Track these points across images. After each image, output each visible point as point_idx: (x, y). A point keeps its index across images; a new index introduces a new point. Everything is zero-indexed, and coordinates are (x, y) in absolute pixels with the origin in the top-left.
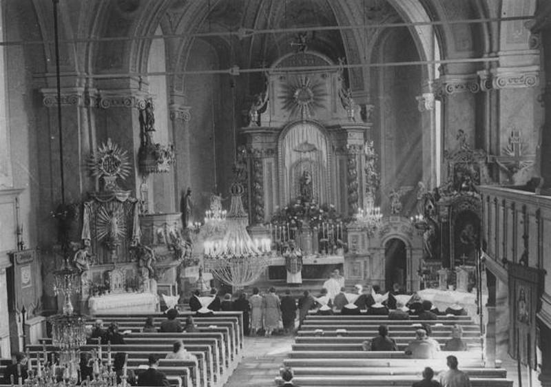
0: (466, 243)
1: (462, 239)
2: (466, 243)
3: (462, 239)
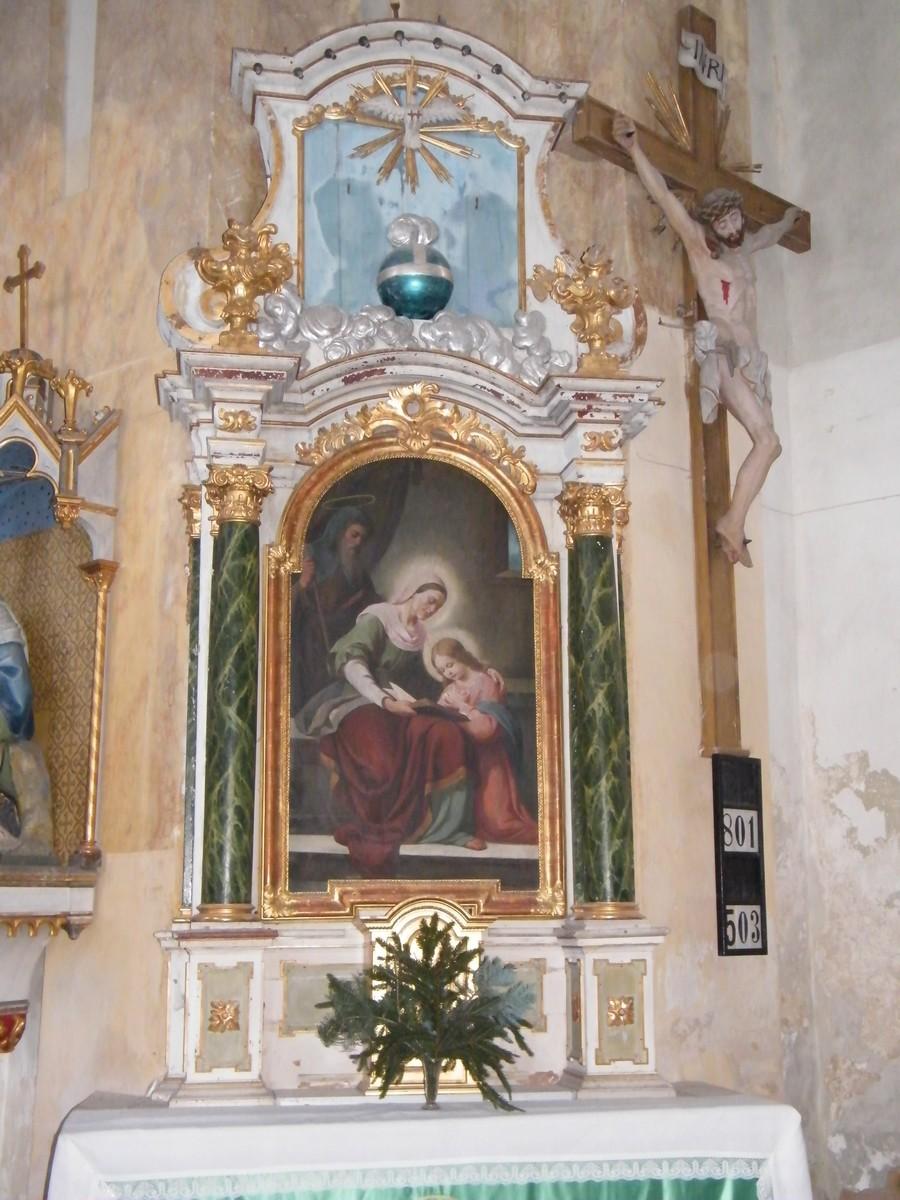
0: (401, 699)
1: (357, 673)
2: (401, 699)
3: (357, 673)
